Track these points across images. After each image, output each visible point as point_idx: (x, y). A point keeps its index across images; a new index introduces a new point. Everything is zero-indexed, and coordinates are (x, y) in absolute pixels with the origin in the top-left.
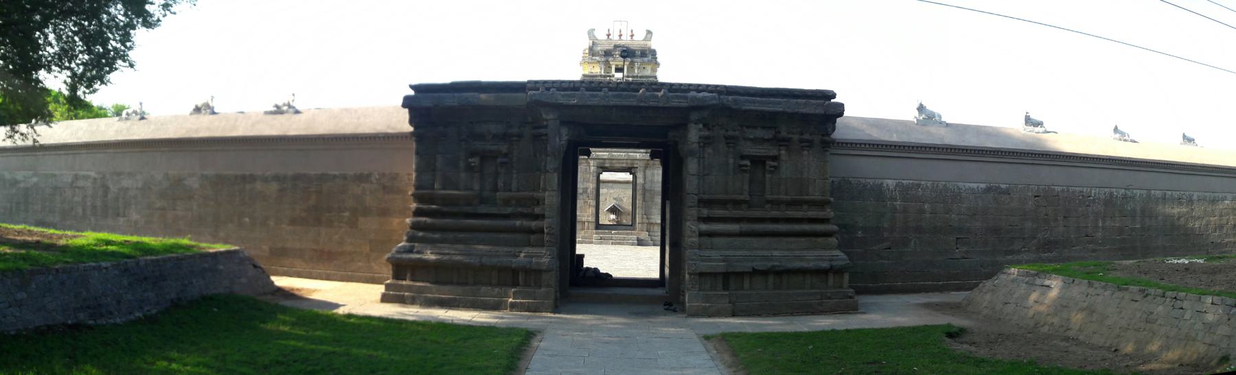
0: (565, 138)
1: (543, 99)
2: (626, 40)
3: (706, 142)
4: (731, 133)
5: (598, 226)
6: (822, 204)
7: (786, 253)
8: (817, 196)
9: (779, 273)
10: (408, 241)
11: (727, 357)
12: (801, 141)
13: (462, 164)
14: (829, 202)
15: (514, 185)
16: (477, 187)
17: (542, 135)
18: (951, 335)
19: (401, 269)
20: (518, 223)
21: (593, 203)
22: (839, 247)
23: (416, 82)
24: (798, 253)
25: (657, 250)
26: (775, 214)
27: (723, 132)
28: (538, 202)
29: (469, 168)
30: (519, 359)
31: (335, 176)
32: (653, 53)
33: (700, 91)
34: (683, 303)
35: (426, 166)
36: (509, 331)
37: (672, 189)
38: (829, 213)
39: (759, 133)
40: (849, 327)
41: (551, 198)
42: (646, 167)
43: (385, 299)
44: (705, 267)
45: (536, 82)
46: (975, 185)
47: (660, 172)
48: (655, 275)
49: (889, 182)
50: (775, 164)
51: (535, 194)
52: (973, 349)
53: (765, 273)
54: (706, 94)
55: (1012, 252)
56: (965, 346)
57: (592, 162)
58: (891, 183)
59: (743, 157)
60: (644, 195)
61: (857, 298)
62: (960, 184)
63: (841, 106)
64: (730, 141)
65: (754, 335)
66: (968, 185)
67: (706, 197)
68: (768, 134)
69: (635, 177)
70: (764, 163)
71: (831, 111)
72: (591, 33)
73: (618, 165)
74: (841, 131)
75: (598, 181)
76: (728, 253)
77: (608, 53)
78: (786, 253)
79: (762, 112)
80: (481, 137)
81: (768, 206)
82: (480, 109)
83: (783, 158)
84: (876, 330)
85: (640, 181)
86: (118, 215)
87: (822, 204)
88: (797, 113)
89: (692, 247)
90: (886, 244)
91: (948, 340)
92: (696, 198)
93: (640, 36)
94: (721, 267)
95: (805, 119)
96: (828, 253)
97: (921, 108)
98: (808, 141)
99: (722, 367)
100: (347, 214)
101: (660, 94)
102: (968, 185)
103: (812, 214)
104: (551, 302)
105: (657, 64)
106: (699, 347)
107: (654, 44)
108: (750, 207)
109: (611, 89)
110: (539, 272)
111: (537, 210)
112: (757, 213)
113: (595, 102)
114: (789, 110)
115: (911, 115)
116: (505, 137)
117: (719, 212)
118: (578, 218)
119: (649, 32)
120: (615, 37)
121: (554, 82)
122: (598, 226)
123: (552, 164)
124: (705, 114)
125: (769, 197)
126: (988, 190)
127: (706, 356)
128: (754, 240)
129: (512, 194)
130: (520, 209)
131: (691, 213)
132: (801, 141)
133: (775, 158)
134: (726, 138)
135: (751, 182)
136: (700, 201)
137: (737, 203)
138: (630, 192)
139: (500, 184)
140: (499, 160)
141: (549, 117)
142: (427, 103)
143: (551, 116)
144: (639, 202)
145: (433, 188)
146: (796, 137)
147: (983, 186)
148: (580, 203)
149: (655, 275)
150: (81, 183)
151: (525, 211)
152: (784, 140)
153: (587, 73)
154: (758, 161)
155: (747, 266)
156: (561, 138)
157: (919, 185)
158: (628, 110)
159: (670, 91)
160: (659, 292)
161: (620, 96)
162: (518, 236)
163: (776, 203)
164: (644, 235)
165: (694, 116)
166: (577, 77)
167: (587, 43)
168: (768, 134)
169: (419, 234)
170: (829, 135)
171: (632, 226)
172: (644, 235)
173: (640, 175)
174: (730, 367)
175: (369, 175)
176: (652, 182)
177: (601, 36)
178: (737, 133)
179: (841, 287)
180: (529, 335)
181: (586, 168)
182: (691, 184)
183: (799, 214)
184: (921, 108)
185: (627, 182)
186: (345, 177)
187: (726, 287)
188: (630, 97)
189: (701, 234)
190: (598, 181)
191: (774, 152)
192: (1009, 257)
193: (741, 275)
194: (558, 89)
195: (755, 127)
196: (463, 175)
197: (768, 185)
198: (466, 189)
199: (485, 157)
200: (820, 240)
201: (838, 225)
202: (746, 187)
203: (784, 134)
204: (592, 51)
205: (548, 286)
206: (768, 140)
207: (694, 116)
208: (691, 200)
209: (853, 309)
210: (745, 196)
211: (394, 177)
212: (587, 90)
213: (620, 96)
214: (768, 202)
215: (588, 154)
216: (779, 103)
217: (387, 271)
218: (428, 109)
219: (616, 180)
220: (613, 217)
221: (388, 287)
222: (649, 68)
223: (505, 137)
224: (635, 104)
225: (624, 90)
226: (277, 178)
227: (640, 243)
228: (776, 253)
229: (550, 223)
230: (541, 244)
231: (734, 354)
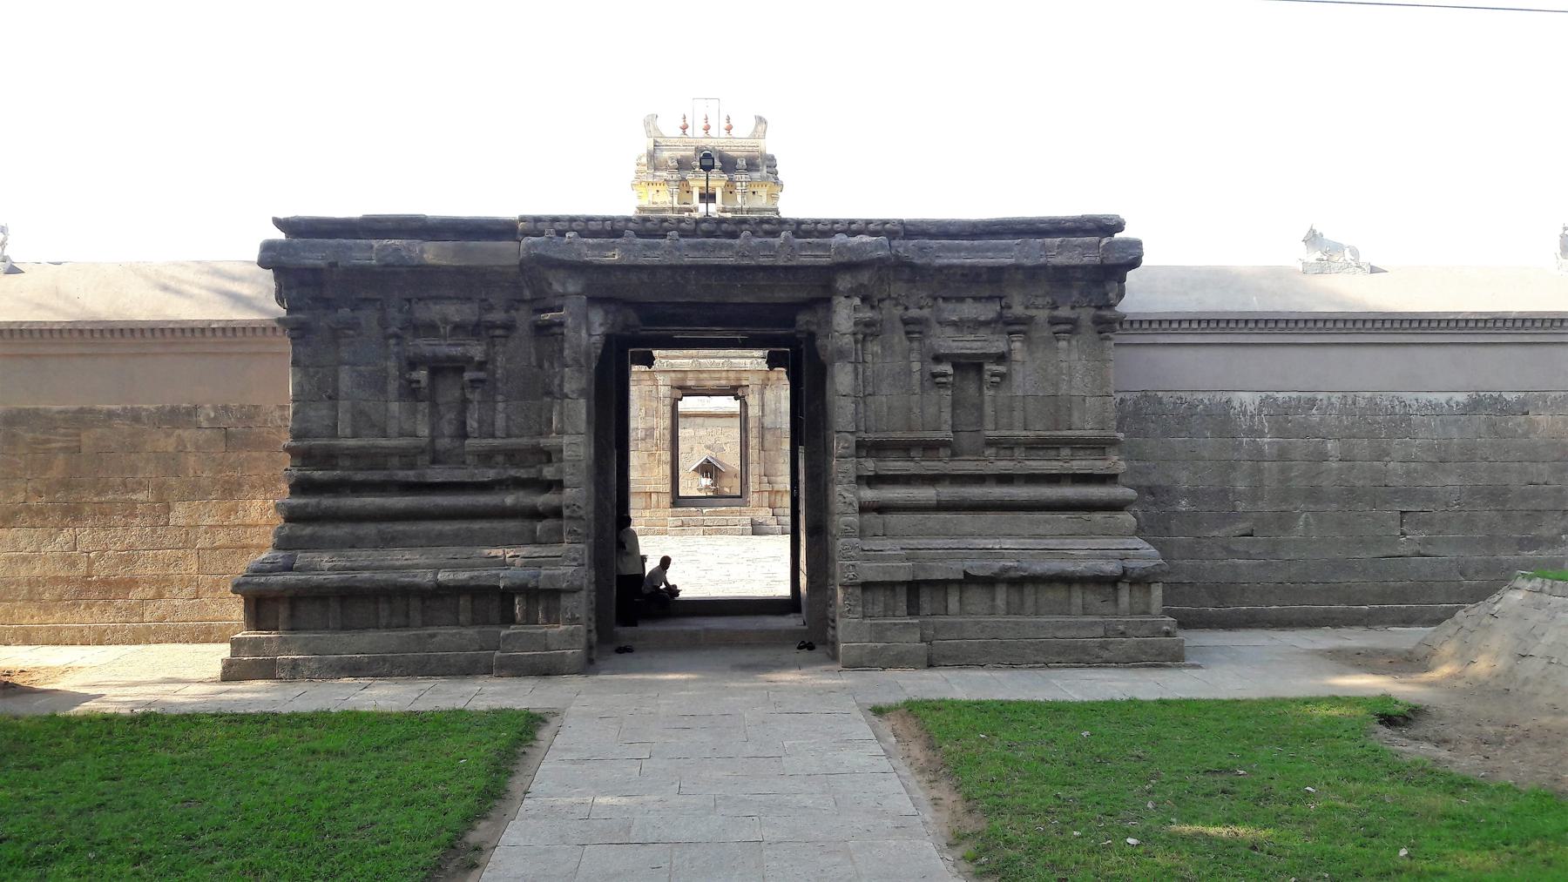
0: (598, 330)
1: (554, 253)
2: (717, 140)
3: (868, 331)
4: (914, 313)
6: (1099, 446)
7: (1029, 543)
8: (1087, 429)
9: (1020, 582)
10: (277, 547)
11: (916, 750)
12: (1054, 322)
13: (393, 386)
14: (1114, 443)
15: (500, 421)
16: (424, 431)
17: (550, 325)
18: (1388, 720)
19: (263, 604)
20: (509, 500)
22: (1139, 531)
23: (283, 215)
24: (1052, 543)
25: (786, 541)
26: (1004, 466)
27: (899, 311)
28: (548, 456)
29: (411, 392)
30: (511, 774)
31: (111, 415)
32: (771, 162)
33: (854, 234)
34: (833, 644)
35: (317, 388)
36: (497, 718)
37: (809, 423)
38: (1115, 462)
39: (969, 310)
40: (1165, 697)
41: (575, 445)
42: (764, 386)
43: (231, 673)
44: (870, 571)
45: (537, 220)
46: (1294, 395)
47: (786, 393)
48: (784, 590)
49: (1246, 396)
50: (1001, 369)
51: (543, 442)
52: (1443, 753)
53: (989, 582)
54: (866, 239)
55: (1535, 543)
56: (1425, 746)
57: (661, 378)
58: (1249, 400)
59: (938, 359)
60: (762, 438)
61: (1182, 635)
62: (1408, 397)
63: (1137, 245)
64: (914, 328)
65: (969, 705)
66: (1424, 397)
67: (871, 436)
68: (987, 311)
69: (744, 405)
70: (979, 368)
71: (1114, 258)
72: (650, 121)
73: (711, 384)
74: (1139, 295)
75: (675, 415)
76: (914, 543)
77: (683, 165)
78: (1029, 543)
79: (972, 267)
80: (430, 329)
81: (990, 452)
82: (425, 275)
83: (1017, 356)
84: (1223, 703)
85: (754, 411)
87: (1099, 446)
88: (1043, 267)
89: (846, 534)
90: (1243, 526)
91: (1383, 731)
92: (852, 438)
93: (743, 129)
94: (902, 571)
95: (1062, 276)
96: (1115, 543)
98: (1067, 321)
99: (906, 772)
101: (777, 241)
102: (1424, 397)
103: (1080, 465)
104: (575, 652)
105: (777, 183)
106: (862, 728)
107: (769, 146)
108: (954, 454)
109: (684, 234)
110: (554, 594)
111: (549, 472)
112: (967, 466)
113: (654, 258)
114: (1028, 262)
115: (1292, 255)
116: (476, 330)
117: (895, 465)
118: (633, 487)
119: (761, 120)
121: (572, 220)
122: (677, 501)
123: (575, 381)
124: (865, 277)
125: (991, 433)
126: (1474, 406)
127: (876, 749)
128: (965, 518)
129: (496, 442)
130: (513, 472)
131: (842, 467)
132: (1054, 322)
133: (1001, 358)
134: (906, 322)
135: (955, 405)
136: (860, 445)
137: (930, 447)
139: (472, 424)
140: (467, 376)
141: (560, 284)
142: (315, 255)
143: (572, 287)
144: (753, 453)
145: (335, 436)
146: (1042, 315)
147: (1461, 397)
148: (635, 459)
149: (784, 590)
151: (522, 473)
152: (1018, 321)
153: (645, 203)
154: (969, 366)
155: (952, 569)
156: (587, 331)
157: (1312, 403)
158: (735, 282)
159: (796, 234)
160: (791, 622)
161: (703, 247)
162: (512, 525)
163: (1004, 445)
164: (764, 515)
165: (844, 282)
166: (629, 210)
167: (647, 144)
168: (987, 311)
169: (302, 526)
170: (1110, 306)
171: (741, 498)
172: (764, 515)
173: (753, 400)
174: (922, 771)
175: (192, 412)
176: (777, 412)
177: (670, 129)
178: (926, 312)
179: (1146, 613)
180: (530, 725)
181: (646, 394)
182: (843, 412)
183: (1054, 467)
184: (1313, 239)
185: (731, 415)
186: (136, 417)
187: (913, 609)
188: (721, 247)
189: (864, 509)
190: (675, 415)
191: (998, 345)
192: (1531, 554)
193: (944, 584)
194: (581, 234)
195: (961, 300)
196: (395, 407)
197: (989, 410)
198: (401, 435)
199: (441, 368)
200: (1098, 517)
201: (1138, 488)
202: (946, 415)
203: (1018, 310)
204: (653, 161)
205: (573, 620)
206: (986, 324)
207: (844, 282)
208: (840, 444)
209: (1173, 658)
210: (945, 434)
211: (250, 414)
212: (639, 234)
213: (703, 247)
214: (990, 443)
215: (648, 361)
216: (1008, 249)
217: (236, 610)
218: (315, 271)
219: (704, 414)
220: (706, 482)
221: (237, 645)
222: (763, 192)
223: (476, 330)
224: (731, 261)
225: (709, 234)
227: (757, 529)
228: (1008, 543)
229: (576, 494)
230: (555, 538)
231: (931, 746)
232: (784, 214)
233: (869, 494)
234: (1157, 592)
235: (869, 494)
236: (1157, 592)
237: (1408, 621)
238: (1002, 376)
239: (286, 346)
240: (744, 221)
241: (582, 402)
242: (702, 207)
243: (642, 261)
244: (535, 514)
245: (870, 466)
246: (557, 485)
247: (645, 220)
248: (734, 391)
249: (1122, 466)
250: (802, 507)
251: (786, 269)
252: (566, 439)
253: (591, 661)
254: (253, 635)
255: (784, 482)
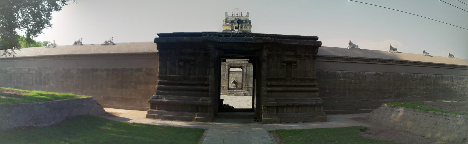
2: (239, 16)
5: (229, 89)
6: (313, 80)
9: (298, 106)
11: (278, 139)
16: (182, 73)
19: (153, 105)
20: (198, 87)
21: (227, 80)
22: (319, 96)
23: (159, 33)
26: (295, 83)
31: (128, 69)
32: (250, 21)
33: (267, 37)
34: (261, 118)
37: (257, 75)
38: (316, 83)
39: (289, 53)
41: (211, 78)
42: (247, 66)
43: (148, 117)
46: (371, 73)
48: (251, 107)
49: (339, 71)
52: (370, 136)
53: (292, 106)
54: (269, 38)
56: (367, 135)
57: (226, 64)
58: (339, 72)
59: (283, 62)
61: (326, 116)
62: (365, 72)
63: (321, 42)
68: (293, 53)
69: (243, 70)
72: (226, 13)
74: (320, 53)
75: (229, 71)
77: (232, 22)
85: (245, 71)
86: (45, 84)
87: (313, 80)
91: (361, 132)
93: (244, 15)
95: (307, 47)
97: (351, 43)
100: (133, 84)
103: (309, 83)
105: (251, 26)
109: (234, 36)
111: (206, 83)
112: (289, 83)
113: (228, 41)
117: (274, 83)
119: (248, 13)
120: (235, 15)
122: (229, 89)
133: (295, 62)
136: (267, 79)
137: (281, 80)
138: (241, 75)
139: (192, 72)
147: (374, 73)
148: (222, 80)
149: (251, 107)
150: (31, 72)
154: (289, 64)
157: (350, 73)
160: (252, 114)
164: (246, 92)
167: (225, 18)
170: (316, 54)
171: (242, 88)
172: (246, 92)
173: (245, 69)
177: (230, 15)
181: (224, 67)
184: (351, 43)
185: (240, 72)
189: (268, 91)
190: (229, 71)
191: (295, 60)
193: (283, 107)
200: (312, 93)
204: (226, 21)
206: (293, 56)
209: (324, 120)
215: (225, 61)
217: (148, 106)
219: (235, 71)
220: (234, 85)
221: (149, 112)
222: (248, 27)
226: (106, 70)
228: (296, 98)
230: (207, 96)
232: (253, 32)
233: (269, 89)
234: (322, 108)
235: (269, 89)
236: (322, 108)
237: (365, 112)
238: (295, 66)
239: (158, 57)
240: (246, 34)
241: (213, 69)
242: (237, 30)
243: (226, 41)
244: (203, 91)
245: (269, 83)
246: (207, 85)
247: (226, 33)
248: (240, 67)
249: (317, 84)
250: (255, 91)
251: (254, 43)
252: (210, 76)
253: (213, 120)
254: (152, 110)
255: (251, 86)
